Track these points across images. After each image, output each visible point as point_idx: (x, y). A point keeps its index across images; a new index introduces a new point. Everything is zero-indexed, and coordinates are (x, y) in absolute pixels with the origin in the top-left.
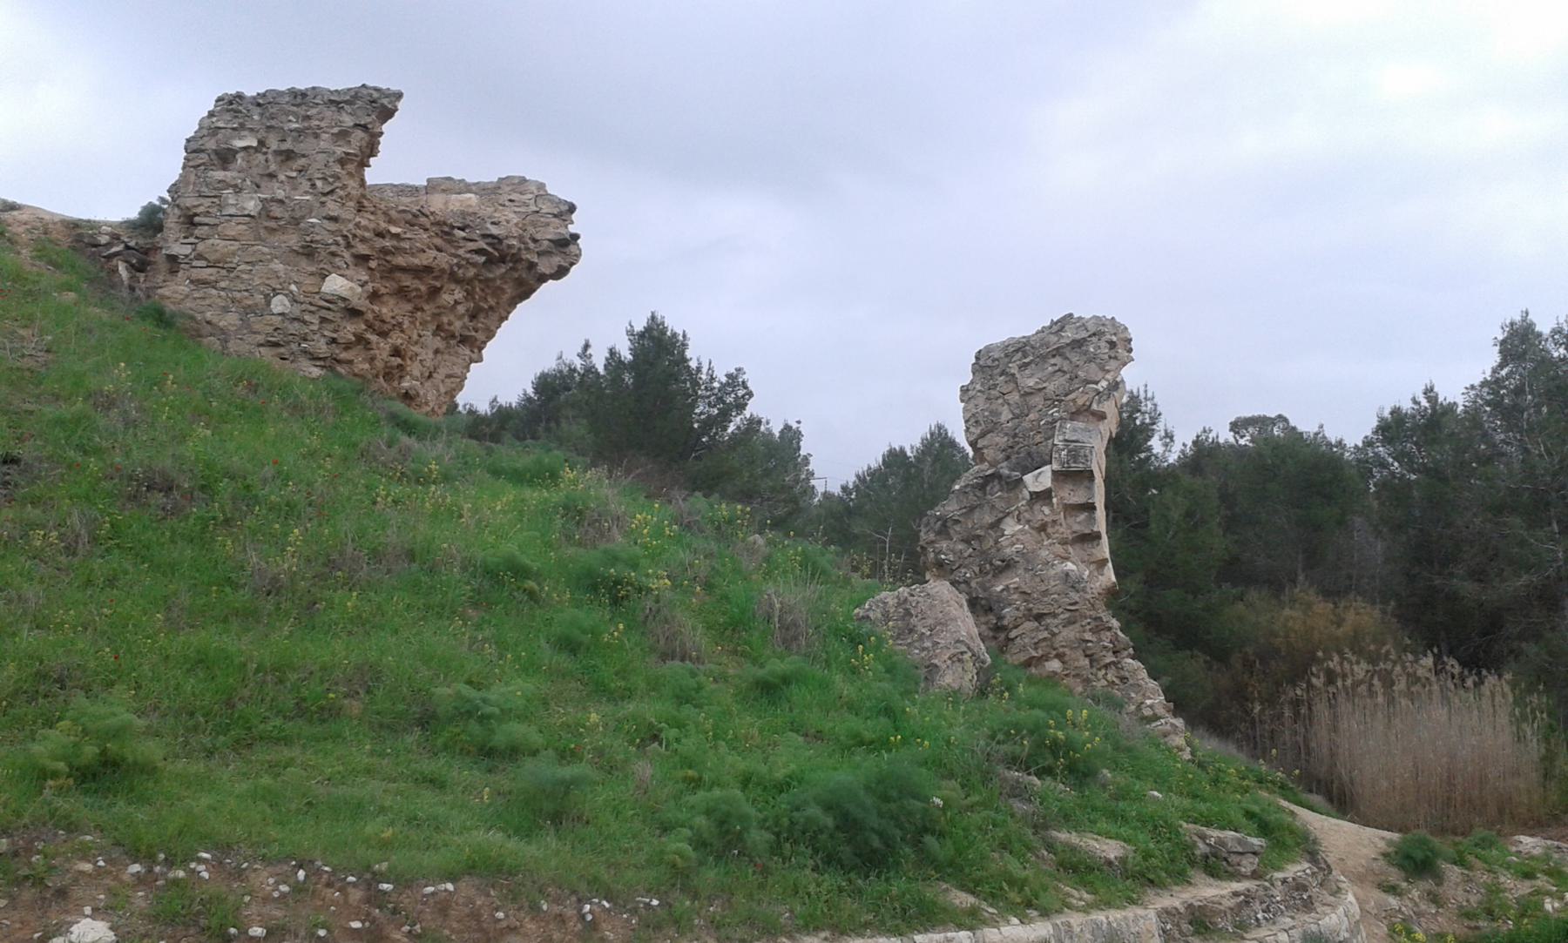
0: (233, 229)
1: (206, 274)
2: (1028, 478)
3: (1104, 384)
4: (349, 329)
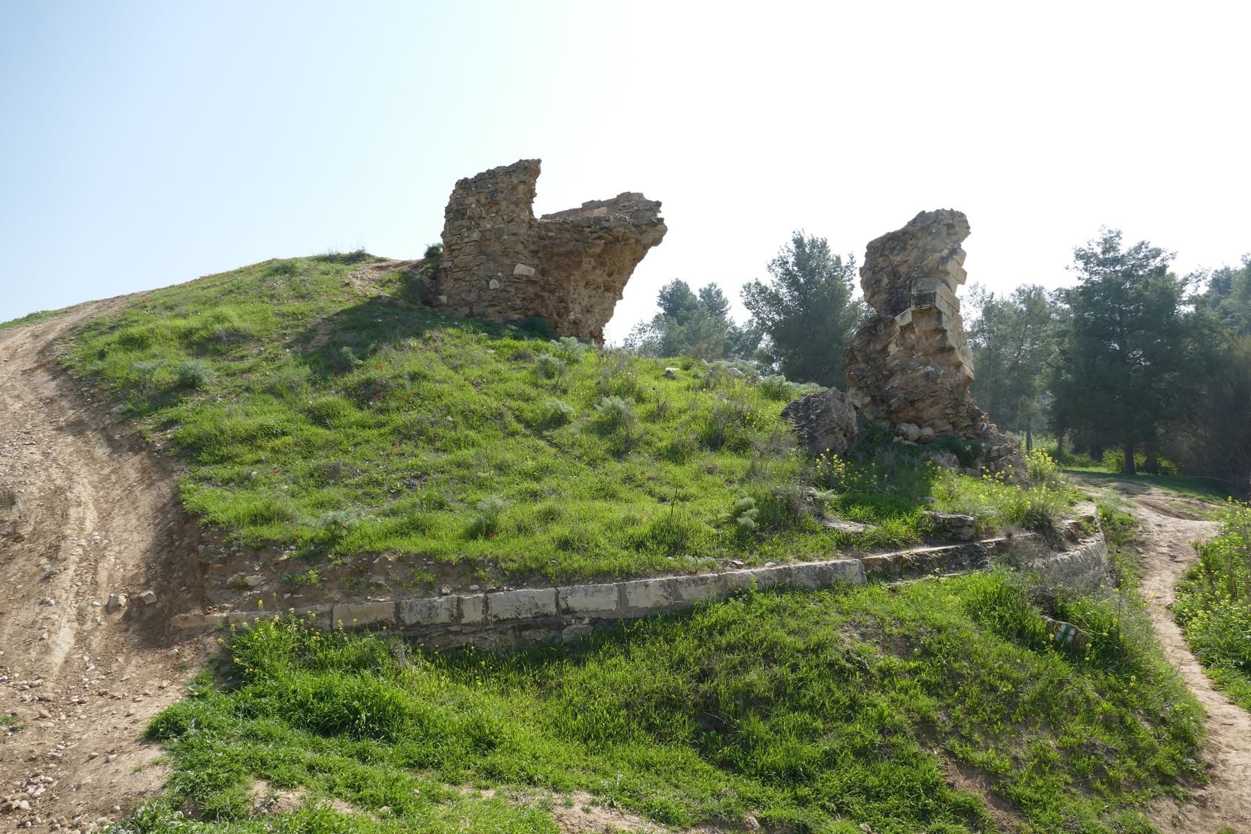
0: (468, 249)
1: (459, 275)
2: (897, 318)
3: (946, 251)
4: (531, 290)
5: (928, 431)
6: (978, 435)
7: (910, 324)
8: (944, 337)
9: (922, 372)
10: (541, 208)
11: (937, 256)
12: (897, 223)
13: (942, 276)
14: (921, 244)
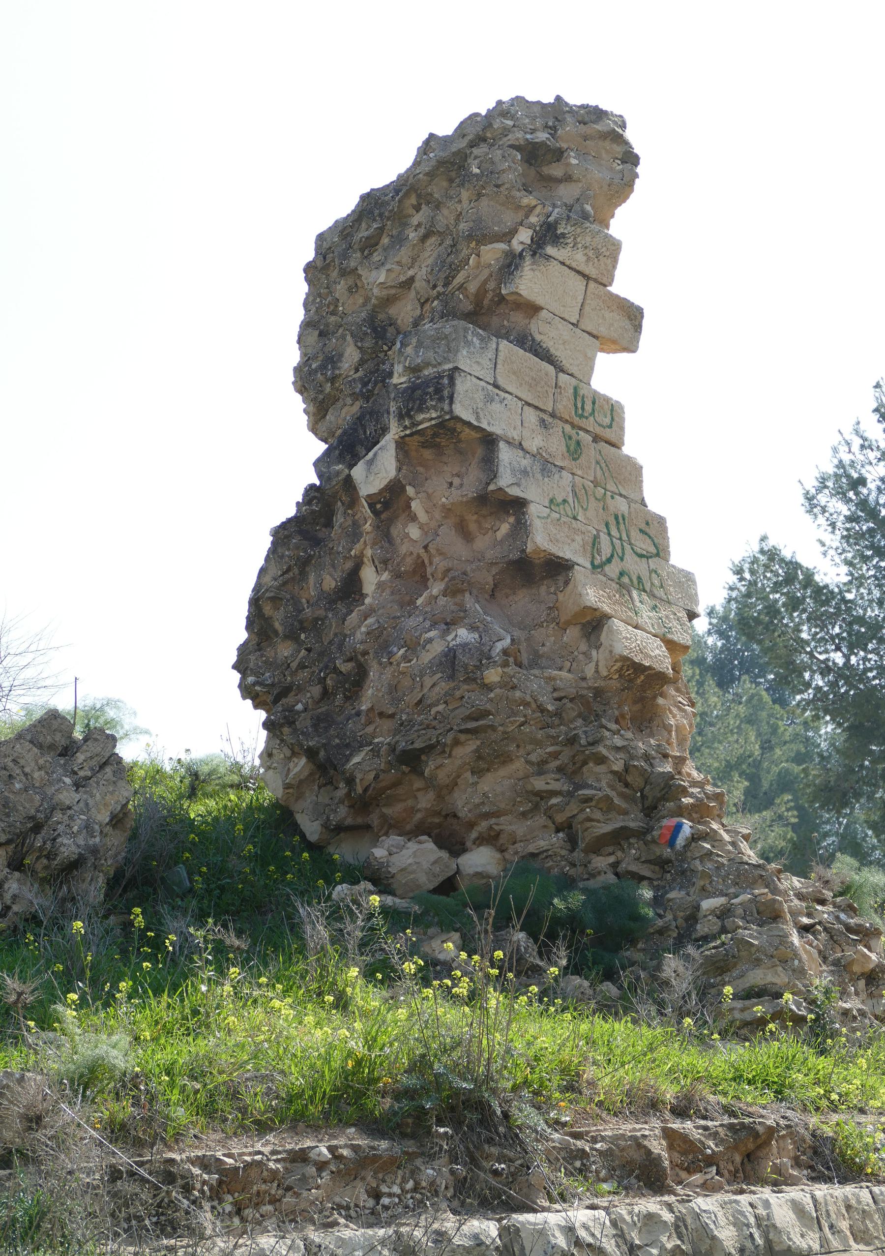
2: (358, 472)
5: (479, 860)
6: (663, 864)
7: (395, 489)
8: (521, 528)
9: (437, 648)
10: (318, 483)
11: (492, 253)
12: (388, 162)
13: (518, 319)
14: (445, 218)
